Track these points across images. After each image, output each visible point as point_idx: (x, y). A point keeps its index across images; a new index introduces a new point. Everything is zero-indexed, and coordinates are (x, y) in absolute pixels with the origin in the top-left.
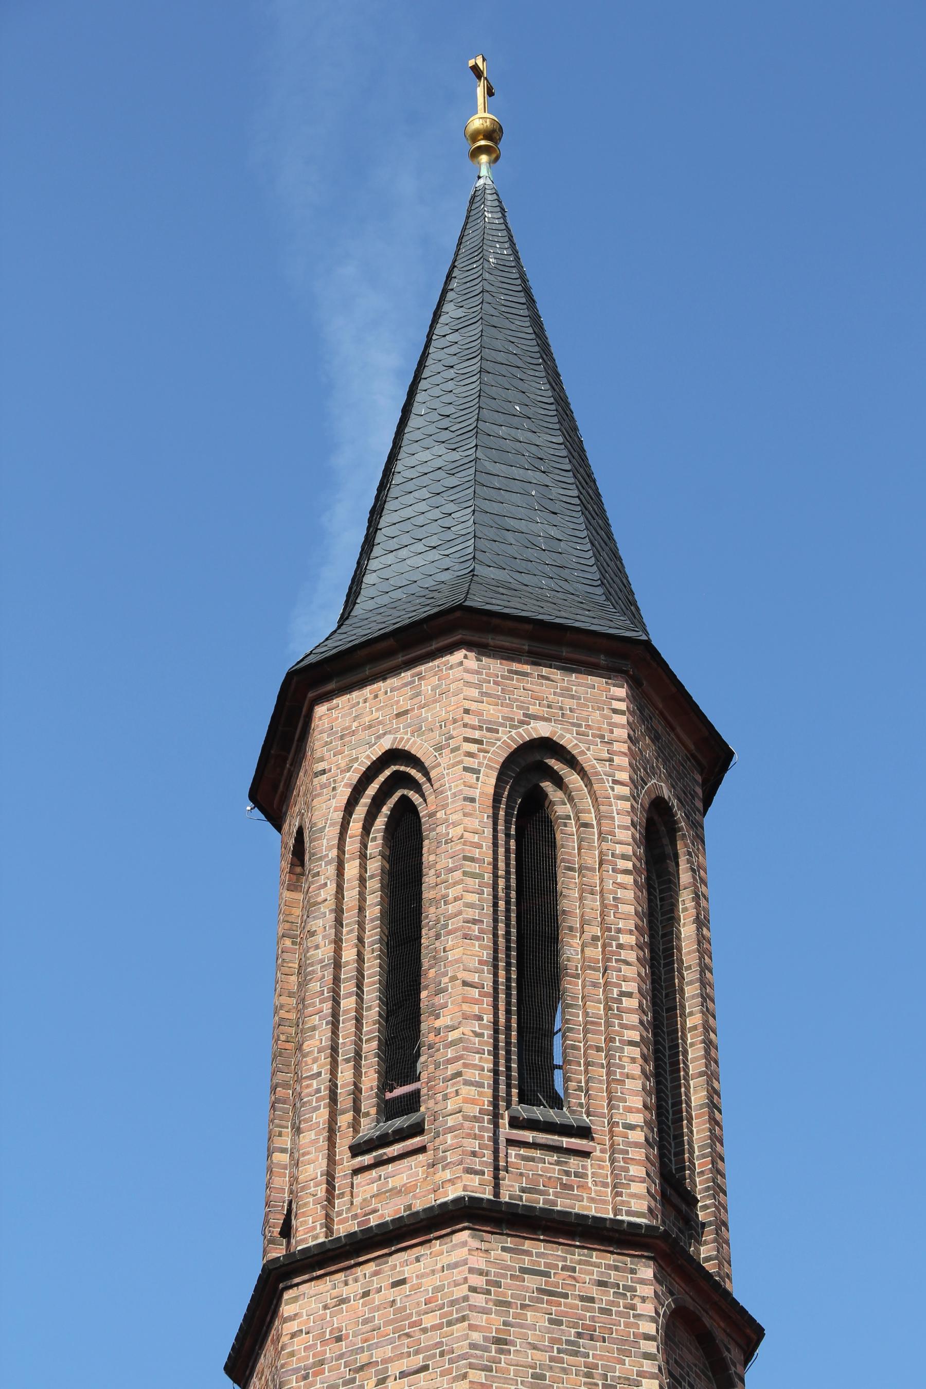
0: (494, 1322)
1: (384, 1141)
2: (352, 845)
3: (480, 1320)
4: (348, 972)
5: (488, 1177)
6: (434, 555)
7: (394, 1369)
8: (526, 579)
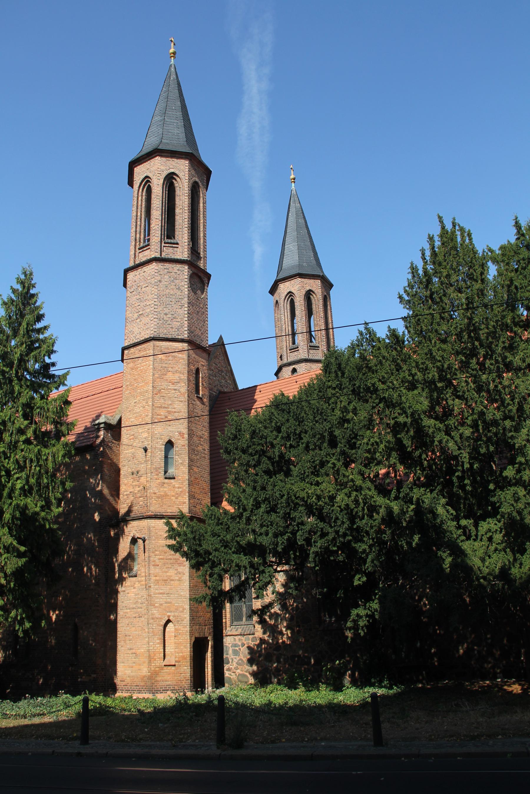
0: (159, 278)
1: (143, 247)
2: (140, 194)
3: (157, 278)
4: (139, 217)
5: (159, 253)
6: (156, 138)
7: (143, 287)
8: (172, 142)
